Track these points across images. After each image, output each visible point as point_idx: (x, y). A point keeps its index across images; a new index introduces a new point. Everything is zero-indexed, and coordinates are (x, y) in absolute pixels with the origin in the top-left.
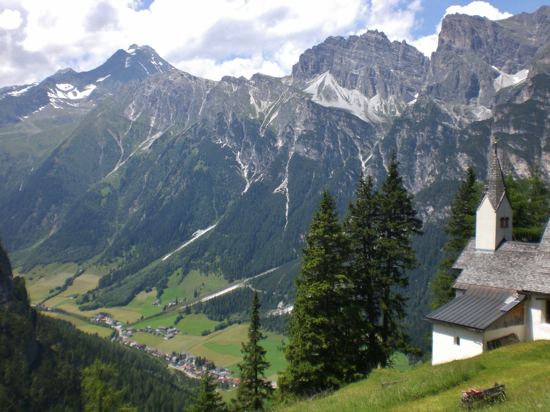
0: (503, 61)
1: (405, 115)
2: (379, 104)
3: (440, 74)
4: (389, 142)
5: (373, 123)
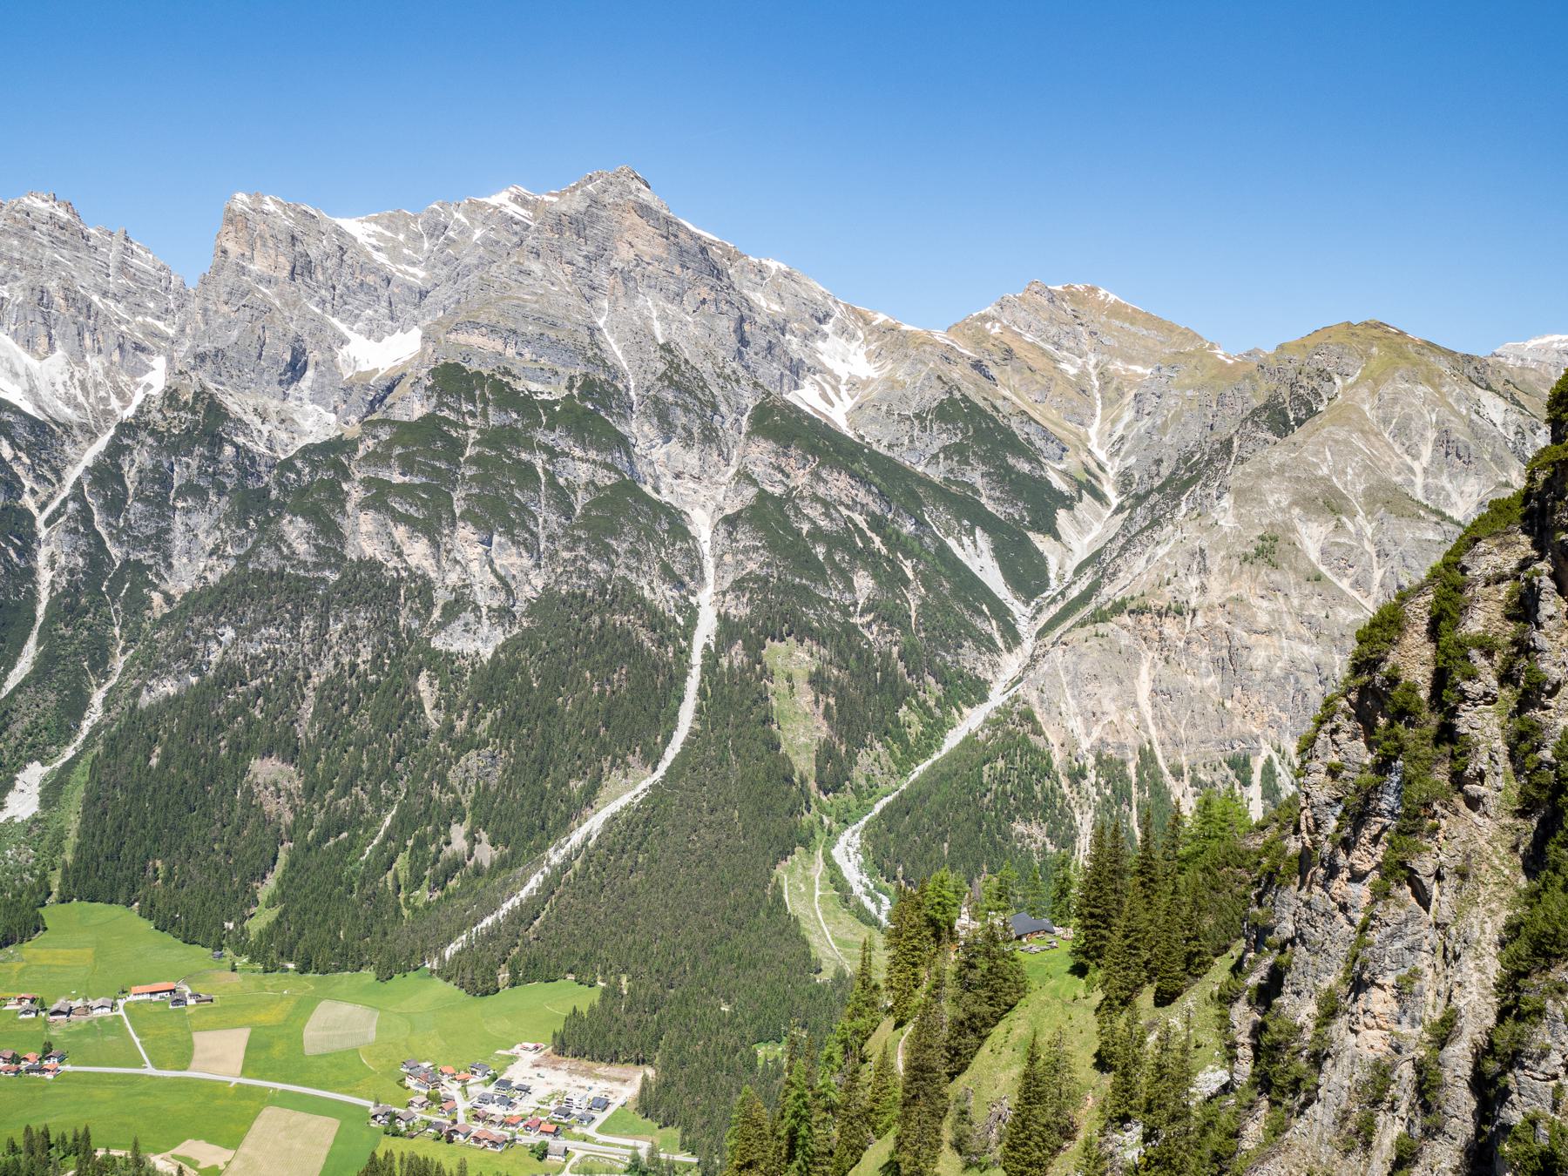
0: (357, 312)
1: (142, 412)
2: (66, 376)
3: (220, 327)
4: (106, 474)
5: (58, 424)
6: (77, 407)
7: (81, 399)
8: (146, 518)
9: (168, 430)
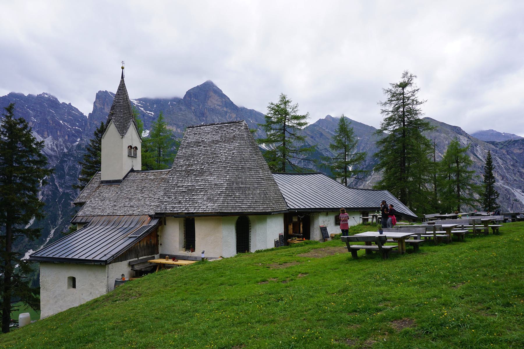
5: (48, 155)
6: (54, 151)
7: (55, 149)
8: (70, 180)
9: (77, 156)
